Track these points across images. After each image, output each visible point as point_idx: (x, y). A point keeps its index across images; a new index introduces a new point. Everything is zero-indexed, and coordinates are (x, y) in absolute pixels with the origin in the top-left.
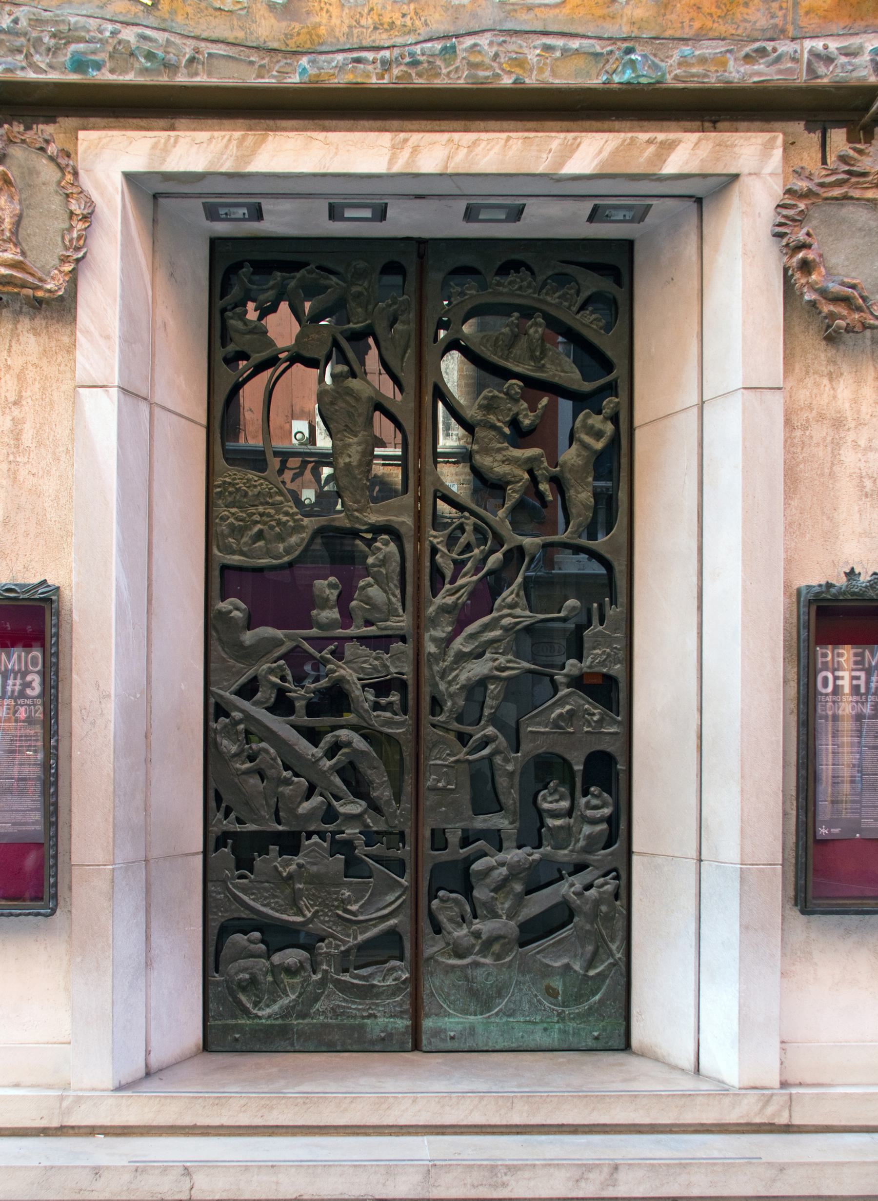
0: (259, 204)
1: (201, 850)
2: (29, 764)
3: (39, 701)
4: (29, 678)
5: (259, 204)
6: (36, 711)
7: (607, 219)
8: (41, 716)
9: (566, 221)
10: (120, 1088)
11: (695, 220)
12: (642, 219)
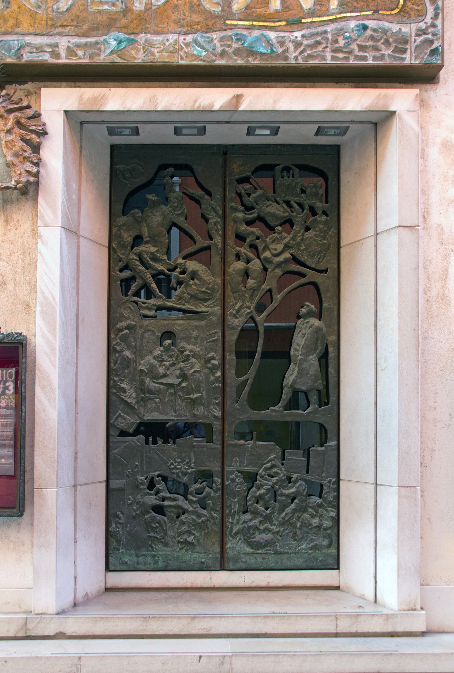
0: (137, 128)
1: (104, 478)
2: (7, 432)
3: (13, 397)
4: (7, 384)
5: (137, 127)
6: (11, 403)
7: (326, 134)
8: (14, 405)
9: (306, 135)
10: (58, 614)
11: (373, 134)
12: (276, 134)
